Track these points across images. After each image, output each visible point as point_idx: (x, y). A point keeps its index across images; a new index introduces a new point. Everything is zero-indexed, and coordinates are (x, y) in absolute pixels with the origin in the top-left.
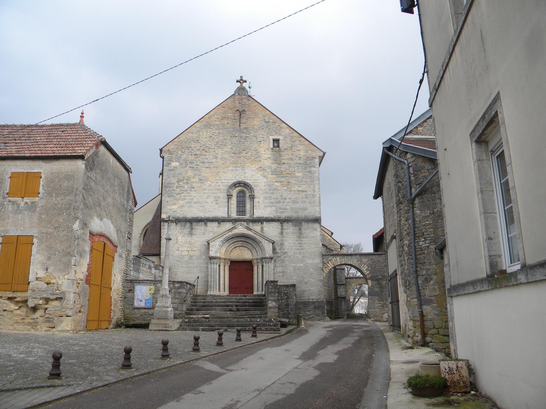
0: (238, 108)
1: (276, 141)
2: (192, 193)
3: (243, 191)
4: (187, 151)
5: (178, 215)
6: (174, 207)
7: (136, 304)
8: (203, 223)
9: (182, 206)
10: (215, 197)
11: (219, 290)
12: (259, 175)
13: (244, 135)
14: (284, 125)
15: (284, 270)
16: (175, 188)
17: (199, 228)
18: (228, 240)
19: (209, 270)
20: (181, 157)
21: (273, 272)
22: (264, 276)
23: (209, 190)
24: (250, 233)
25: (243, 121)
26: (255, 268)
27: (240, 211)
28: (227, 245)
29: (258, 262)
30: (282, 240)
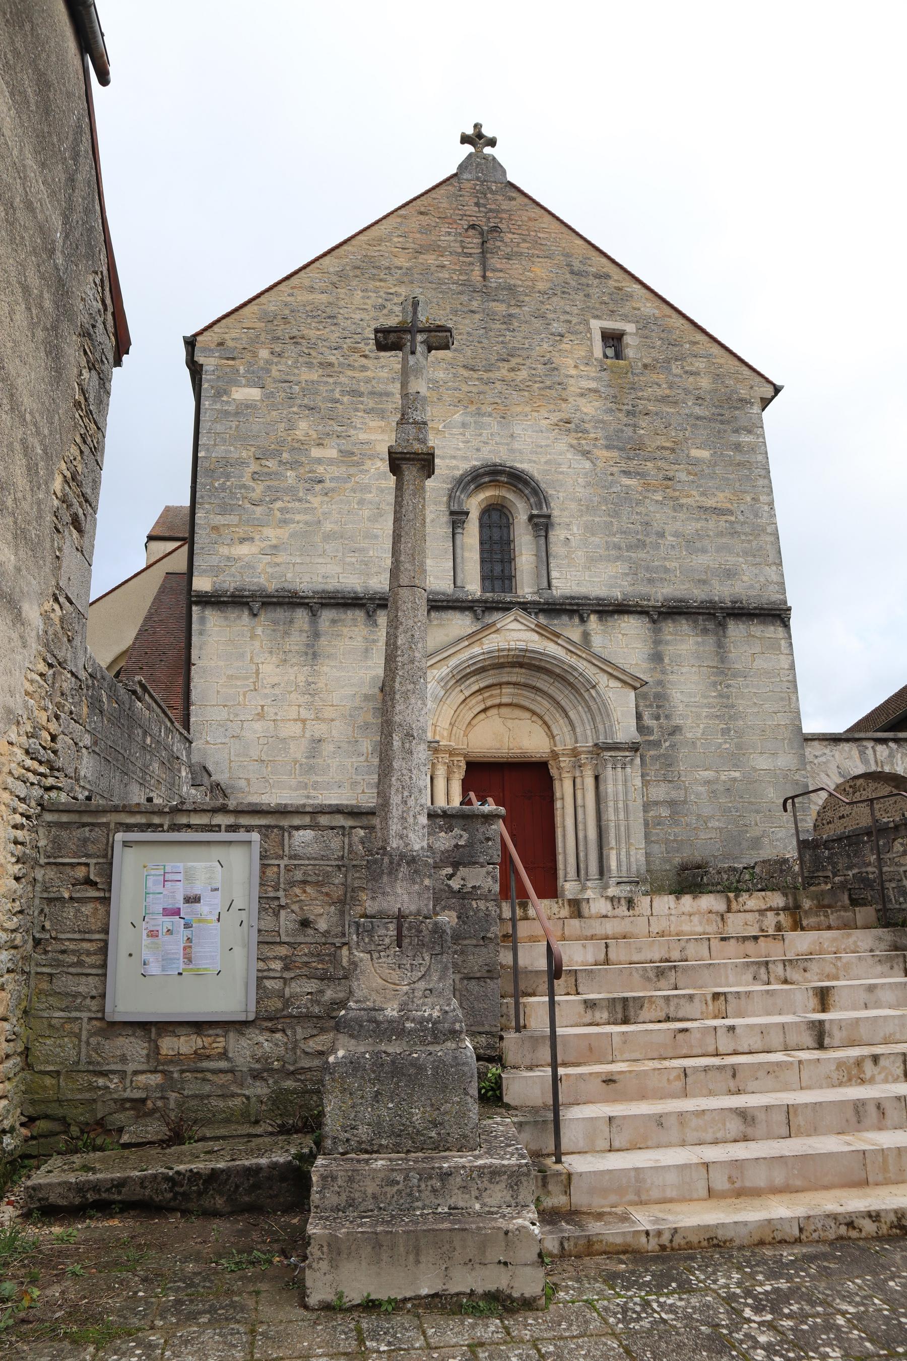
0: (473, 220)
1: (613, 339)
2: (316, 501)
3: (505, 502)
4: (291, 351)
5: (262, 580)
6: (243, 550)
7: (129, 999)
8: (360, 614)
9: (275, 547)
13: (500, 308)
14: (637, 287)
15: (674, 794)
16: (247, 480)
20: (268, 371)
21: (639, 802)
24: (551, 648)
25: (494, 261)
26: (564, 789)
28: (457, 697)
30: (660, 683)
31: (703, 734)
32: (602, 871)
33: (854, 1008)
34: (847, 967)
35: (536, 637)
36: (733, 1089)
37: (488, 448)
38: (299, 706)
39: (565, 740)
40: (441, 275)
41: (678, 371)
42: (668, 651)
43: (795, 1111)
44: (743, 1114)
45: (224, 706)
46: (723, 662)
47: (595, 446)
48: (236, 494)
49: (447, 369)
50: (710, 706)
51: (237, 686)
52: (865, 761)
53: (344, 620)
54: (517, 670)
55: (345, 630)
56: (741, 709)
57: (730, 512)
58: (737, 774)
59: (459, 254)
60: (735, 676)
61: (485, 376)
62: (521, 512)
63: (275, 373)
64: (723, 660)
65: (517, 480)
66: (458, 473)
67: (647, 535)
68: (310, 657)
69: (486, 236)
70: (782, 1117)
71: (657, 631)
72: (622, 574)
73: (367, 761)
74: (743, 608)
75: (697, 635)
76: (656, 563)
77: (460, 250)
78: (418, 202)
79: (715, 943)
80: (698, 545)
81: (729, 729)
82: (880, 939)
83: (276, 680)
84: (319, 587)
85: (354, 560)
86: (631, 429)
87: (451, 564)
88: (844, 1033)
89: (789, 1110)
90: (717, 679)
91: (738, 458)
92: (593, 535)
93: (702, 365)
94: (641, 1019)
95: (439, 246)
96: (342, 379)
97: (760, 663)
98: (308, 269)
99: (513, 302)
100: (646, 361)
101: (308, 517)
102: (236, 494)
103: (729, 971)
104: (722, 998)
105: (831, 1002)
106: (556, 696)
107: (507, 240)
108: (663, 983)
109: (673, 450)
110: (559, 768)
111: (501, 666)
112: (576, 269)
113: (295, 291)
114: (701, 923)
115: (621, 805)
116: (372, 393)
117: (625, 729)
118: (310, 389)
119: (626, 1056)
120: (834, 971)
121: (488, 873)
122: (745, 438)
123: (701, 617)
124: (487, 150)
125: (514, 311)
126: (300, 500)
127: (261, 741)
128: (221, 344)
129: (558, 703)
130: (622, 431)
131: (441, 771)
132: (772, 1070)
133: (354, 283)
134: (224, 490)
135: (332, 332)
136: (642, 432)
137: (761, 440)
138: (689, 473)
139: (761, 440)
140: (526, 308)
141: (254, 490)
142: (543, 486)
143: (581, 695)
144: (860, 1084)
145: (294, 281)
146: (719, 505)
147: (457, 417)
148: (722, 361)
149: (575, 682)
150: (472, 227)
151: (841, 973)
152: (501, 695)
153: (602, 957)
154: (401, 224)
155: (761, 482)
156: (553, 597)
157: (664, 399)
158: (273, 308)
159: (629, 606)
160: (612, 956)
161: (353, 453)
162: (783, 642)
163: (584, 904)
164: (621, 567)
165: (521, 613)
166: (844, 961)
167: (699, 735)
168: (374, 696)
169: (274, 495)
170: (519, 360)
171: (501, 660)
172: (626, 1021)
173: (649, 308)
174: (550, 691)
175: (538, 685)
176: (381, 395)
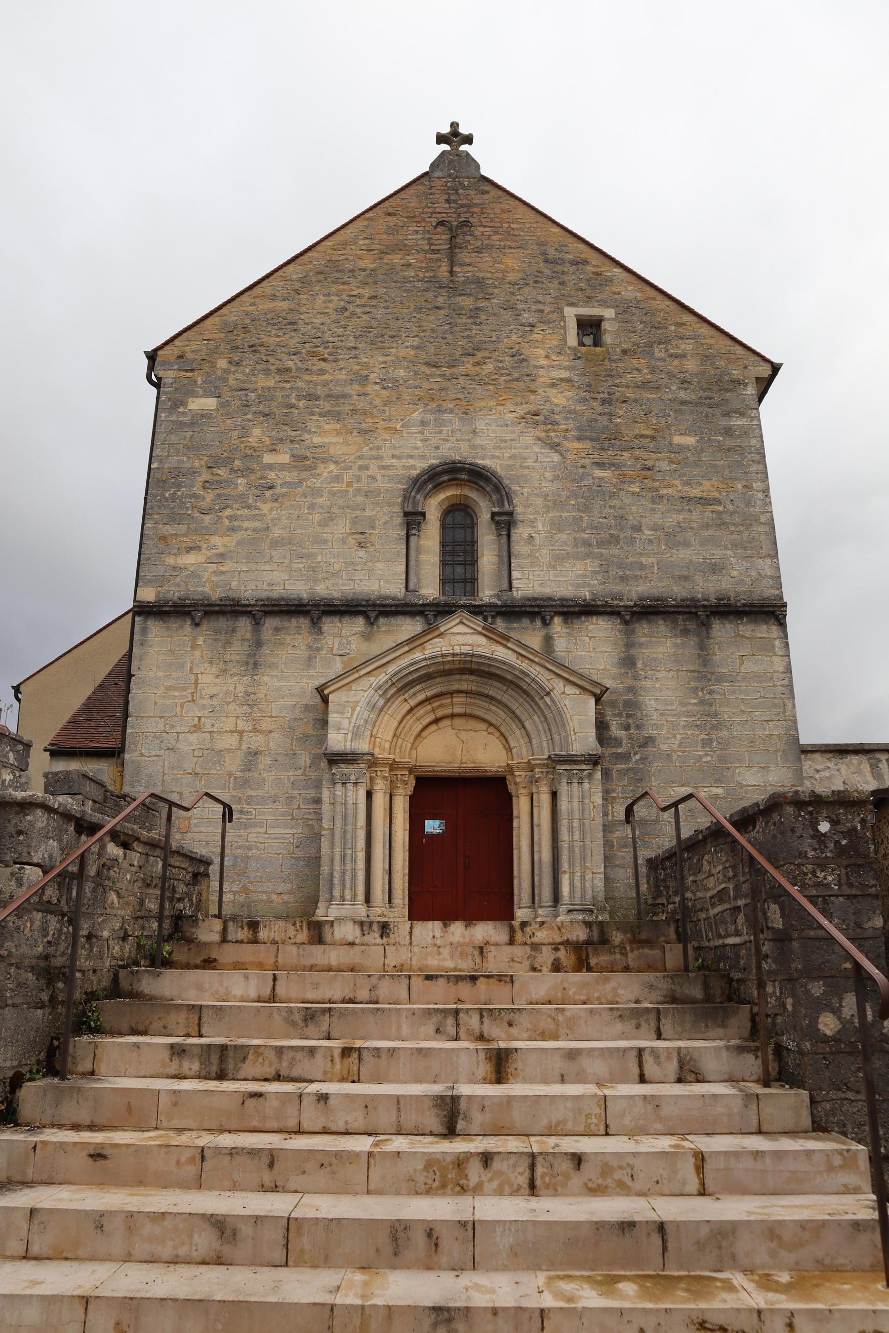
1: (590, 327)
2: (265, 508)
3: (462, 502)
4: (250, 359)
6: (190, 559)
8: (304, 622)
9: (222, 555)
10: (354, 522)
11: (368, 900)
12: (528, 439)
13: (467, 302)
14: (618, 270)
16: (197, 489)
17: (291, 643)
18: (404, 684)
19: (326, 808)
20: (225, 380)
21: (599, 820)
22: (564, 835)
23: (333, 494)
24: (501, 653)
25: (463, 256)
26: (521, 806)
27: (453, 581)
28: (400, 707)
29: (535, 781)
30: (631, 690)
31: (680, 746)
32: (556, 898)
33: (546, 1081)
34: (572, 1023)
35: (483, 641)
36: (268, 1183)
37: (448, 445)
38: (237, 717)
39: (522, 753)
40: (406, 274)
41: (662, 355)
42: (643, 654)
43: (299, 1228)
44: (221, 1225)
45: (161, 717)
46: (705, 666)
47: (565, 437)
48: (185, 503)
49: (408, 367)
50: (689, 714)
51: (175, 697)
52: (878, 776)
53: (287, 628)
54: (466, 677)
55: (288, 638)
56: (726, 717)
57: (718, 502)
58: (720, 791)
59: (426, 252)
60: (719, 680)
61: (448, 372)
62: (484, 510)
63: (231, 382)
64: (705, 663)
65: (478, 477)
66: (414, 473)
67: (621, 530)
68: (250, 666)
69: (455, 232)
70: (278, 1235)
71: (629, 633)
72: (592, 572)
73: (304, 774)
74: (729, 606)
75: (676, 636)
76: (631, 559)
77: (427, 248)
78: (387, 203)
79: (417, 982)
80: (679, 538)
81: (711, 741)
82: (651, 987)
83: (214, 691)
84: (264, 595)
85: (301, 566)
86: (606, 418)
87: (403, 567)
88: (488, 1116)
89: (290, 1225)
90: (697, 684)
91: (728, 443)
92: (560, 531)
93: (689, 348)
94: (242, 1075)
95: (406, 245)
96: (300, 384)
97: (750, 666)
98: (271, 278)
99: (481, 296)
100: (624, 346)
101: (256, 524)
102: (185, 503)
103: (404, 1019)
104: (355, 1055)
105: (511, 1070)
106: (511, 705)
107: (477, 233)
108: (312, 1029)
109: (653, 438)
110: (516, 784)
111: (448, 673)
112: (550, 257)
113: (257, 300)
114: (452, 957)
115: (576, 824)
116: (329, 396)
117: (582, 737)
118: (266, 395)
119: (176, 1123)
120: (552, 1027)
121: (13, 874)
122: (737, 422)
123: (681, 617)
124: (464, 148)
125: (480, 304)
126: (249, 507)
127: (196, 753)
128: (181, 357)
129: (514, 713)
130: (596, 421)
131: (380, 787)
132: (328, 1162)
133: (317, 288)
134: (174, 500)
135: (292, 337)
136: (619, 420)
137: (755, 422)
138: (671, 462)
139: (755, 422)
140: (495, 301)
141: (204, 499)
142: (506, 482)
143: (536, 703)
144: (458, 1194)
145: (257, 291)
146: (705, 494)
147: (416, 416)
148: (712, 341)
149: (529, 689)
150: (441, 223)
151: (563, 1032)
152: (452, 704)
153: (267, 991)
154: (367, 226)
155: (754, 468)
156: (513, 598)
157: (645, 385)
158: (234, 319)
159: (597, 606)
160: (281, 990)
161: (306, 458)
162: (777, 642)
163: (327, 928)
164: (590, 565)
165: (466, 614)
166: (568, 1014)
167: (675, 747)
168: (314, 706)
169: (224, 503)
170: (486, 354)
171: (447, 667)
172: (221, 1076)
173: (630, 292)
174: (504, 700)
175: (491, 693)
176: (337, 397)
